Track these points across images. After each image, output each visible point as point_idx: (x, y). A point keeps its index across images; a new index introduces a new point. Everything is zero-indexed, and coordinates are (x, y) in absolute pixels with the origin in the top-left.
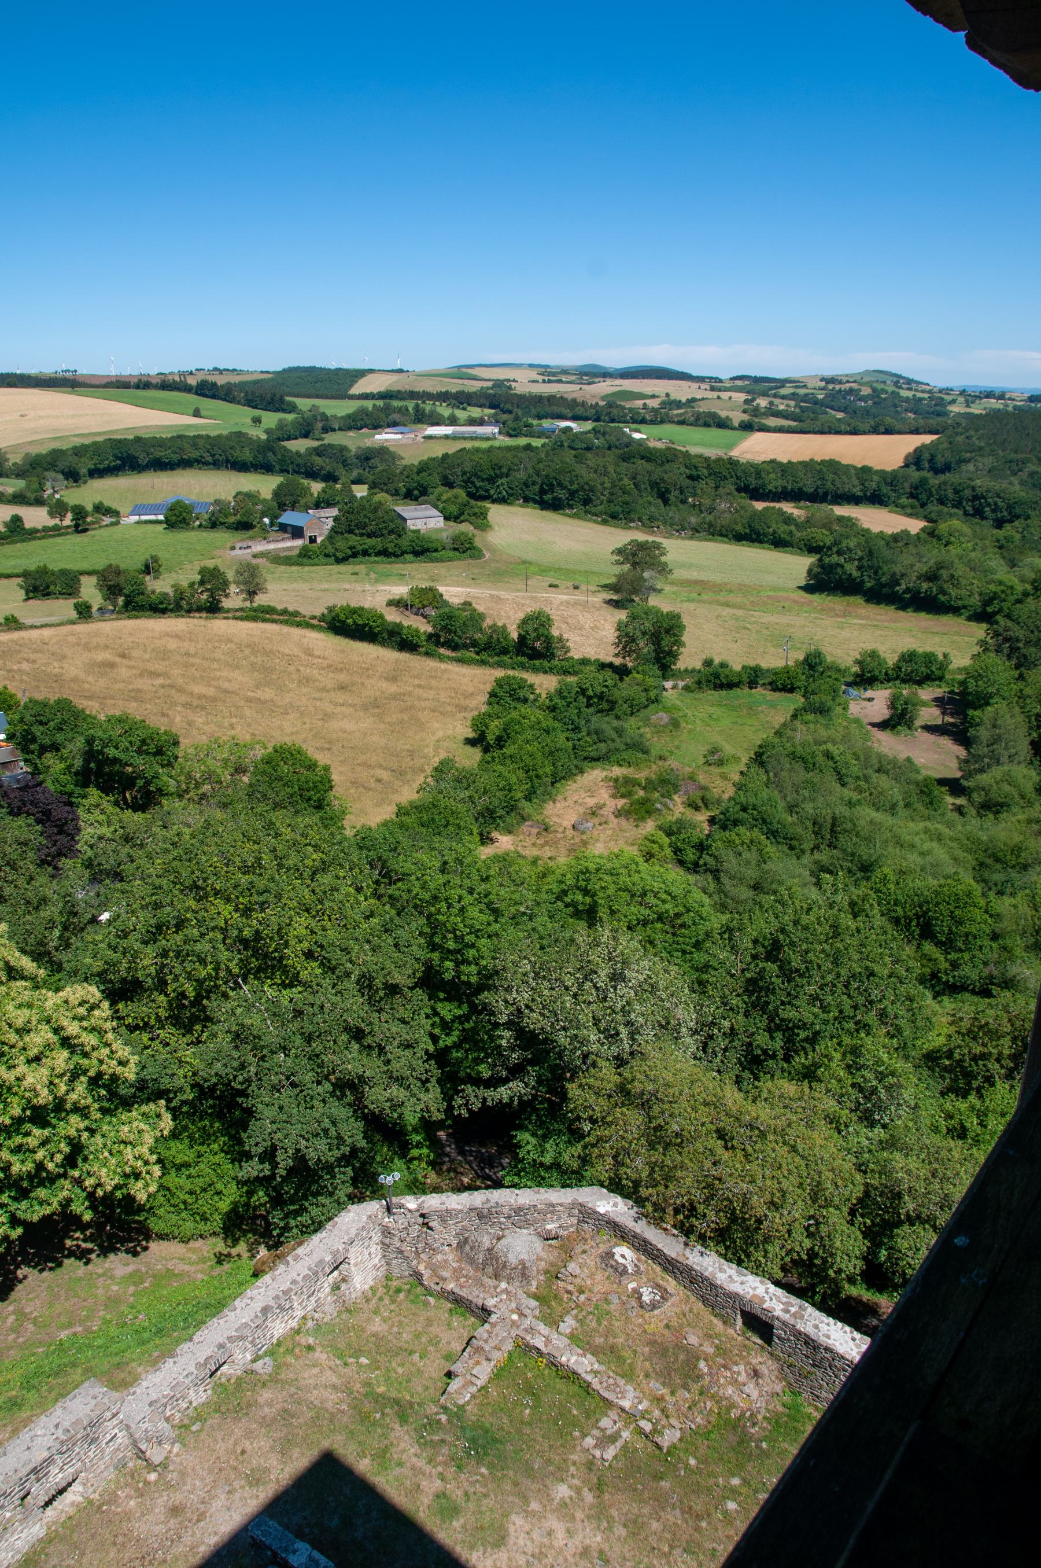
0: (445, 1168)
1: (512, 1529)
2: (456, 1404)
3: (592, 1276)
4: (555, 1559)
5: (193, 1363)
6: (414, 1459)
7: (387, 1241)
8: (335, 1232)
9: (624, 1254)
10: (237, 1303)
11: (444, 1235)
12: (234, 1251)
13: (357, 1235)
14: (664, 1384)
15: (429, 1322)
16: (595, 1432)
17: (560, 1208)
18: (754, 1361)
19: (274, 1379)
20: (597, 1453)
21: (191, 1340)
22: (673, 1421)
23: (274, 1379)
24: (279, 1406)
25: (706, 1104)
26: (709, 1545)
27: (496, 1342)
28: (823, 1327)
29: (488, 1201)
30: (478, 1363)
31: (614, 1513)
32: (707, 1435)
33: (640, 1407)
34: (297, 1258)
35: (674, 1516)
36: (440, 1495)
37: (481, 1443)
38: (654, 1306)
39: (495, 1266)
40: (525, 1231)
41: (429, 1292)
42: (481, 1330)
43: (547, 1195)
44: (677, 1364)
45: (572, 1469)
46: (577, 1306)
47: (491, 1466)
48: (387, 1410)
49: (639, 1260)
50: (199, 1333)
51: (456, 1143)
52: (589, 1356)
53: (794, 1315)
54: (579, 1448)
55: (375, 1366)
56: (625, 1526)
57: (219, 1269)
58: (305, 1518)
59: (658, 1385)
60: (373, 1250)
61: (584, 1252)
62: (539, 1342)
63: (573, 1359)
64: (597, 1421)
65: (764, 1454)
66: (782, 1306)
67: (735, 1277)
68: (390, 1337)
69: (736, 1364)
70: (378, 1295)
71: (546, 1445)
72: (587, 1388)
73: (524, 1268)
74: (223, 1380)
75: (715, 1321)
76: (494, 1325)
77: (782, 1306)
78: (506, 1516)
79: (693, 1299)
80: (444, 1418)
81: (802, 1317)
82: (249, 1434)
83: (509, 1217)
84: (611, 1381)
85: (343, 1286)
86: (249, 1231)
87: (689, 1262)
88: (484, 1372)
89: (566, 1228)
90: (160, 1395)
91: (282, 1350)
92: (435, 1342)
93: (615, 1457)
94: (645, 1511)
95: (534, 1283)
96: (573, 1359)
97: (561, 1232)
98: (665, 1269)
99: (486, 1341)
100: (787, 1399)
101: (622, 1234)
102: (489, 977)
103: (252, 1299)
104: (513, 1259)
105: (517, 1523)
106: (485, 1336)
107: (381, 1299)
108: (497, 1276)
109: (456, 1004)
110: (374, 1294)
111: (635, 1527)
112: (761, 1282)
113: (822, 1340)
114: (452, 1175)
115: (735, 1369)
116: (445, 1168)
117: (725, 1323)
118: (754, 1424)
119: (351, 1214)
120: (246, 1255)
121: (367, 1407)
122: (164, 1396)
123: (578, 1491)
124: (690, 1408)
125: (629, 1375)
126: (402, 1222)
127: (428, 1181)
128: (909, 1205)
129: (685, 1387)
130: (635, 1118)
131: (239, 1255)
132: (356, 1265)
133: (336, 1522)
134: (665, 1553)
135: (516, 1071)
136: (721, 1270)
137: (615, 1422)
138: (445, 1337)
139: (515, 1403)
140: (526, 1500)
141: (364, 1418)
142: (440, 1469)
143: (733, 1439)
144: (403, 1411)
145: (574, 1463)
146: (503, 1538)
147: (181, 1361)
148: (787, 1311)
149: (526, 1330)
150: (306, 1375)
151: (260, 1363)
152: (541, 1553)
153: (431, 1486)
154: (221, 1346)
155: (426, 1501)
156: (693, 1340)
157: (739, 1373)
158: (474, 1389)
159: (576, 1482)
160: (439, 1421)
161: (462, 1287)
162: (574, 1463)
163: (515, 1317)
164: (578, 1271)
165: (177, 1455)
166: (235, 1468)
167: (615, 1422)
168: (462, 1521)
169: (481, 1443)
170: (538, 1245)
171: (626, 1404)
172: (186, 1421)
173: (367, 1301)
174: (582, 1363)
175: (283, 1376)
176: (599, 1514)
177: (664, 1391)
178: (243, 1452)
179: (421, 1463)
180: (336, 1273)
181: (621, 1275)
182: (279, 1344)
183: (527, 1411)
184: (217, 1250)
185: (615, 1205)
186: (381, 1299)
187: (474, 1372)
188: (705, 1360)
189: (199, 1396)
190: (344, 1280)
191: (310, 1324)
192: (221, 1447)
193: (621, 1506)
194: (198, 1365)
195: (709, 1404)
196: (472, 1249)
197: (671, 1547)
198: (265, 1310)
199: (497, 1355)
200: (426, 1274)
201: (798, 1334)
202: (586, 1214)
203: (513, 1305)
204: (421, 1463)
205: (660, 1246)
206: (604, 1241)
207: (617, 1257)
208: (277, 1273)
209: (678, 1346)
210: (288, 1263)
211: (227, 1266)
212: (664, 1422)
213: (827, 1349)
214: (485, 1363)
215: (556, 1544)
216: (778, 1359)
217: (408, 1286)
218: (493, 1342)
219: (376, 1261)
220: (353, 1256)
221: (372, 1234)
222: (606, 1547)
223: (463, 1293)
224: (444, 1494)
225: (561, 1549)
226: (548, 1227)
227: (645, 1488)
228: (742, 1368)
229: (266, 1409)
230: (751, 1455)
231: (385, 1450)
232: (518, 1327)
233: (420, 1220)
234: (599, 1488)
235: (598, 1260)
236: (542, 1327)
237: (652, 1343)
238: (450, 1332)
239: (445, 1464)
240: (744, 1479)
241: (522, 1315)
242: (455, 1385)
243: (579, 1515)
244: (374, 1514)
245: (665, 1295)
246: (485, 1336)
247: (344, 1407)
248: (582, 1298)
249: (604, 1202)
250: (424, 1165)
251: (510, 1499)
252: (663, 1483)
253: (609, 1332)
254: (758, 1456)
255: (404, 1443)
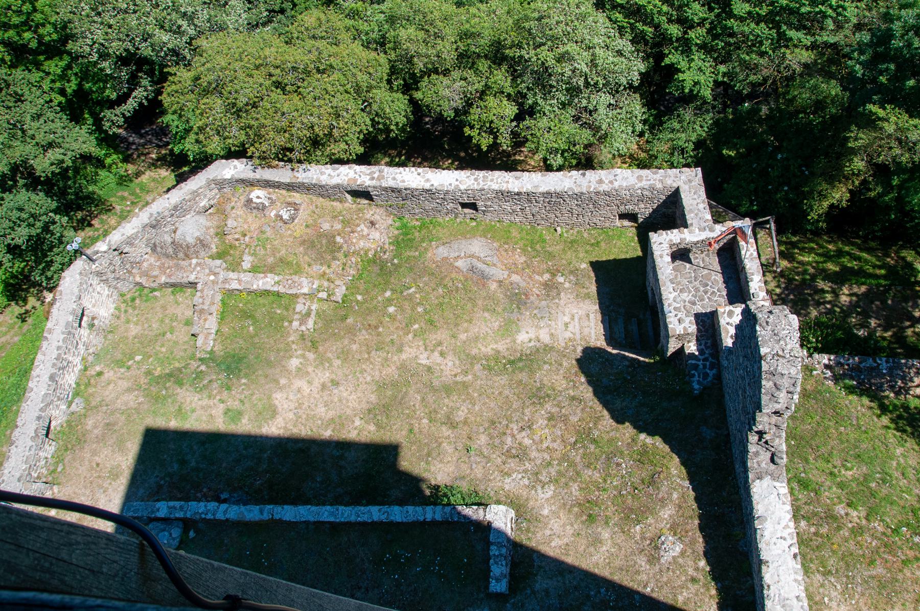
0: (135, 156)
1: (277, 402)
2: (207, 352)
3: (246, 221)
4: (309, 402)
5: (28, 440)
6: (200, 403)
7: (104, 278)
8: (64, 297)
9: (258, 195)
10: (31, 384)
11: (140, 251)
12: (29, 307)
13: (80, 291)
14: (321, 264)
15: (164, 308)
16: (296, 316)
17: (201, 190)
18: (368, 216)
19: (90, 408)
20: (303, 328)
21: (17, 427)
22: (337, 283)
23: (90, 408)
24: (102, 425)
25: (257, 67)
26: (388, 340)
27: (209, 298)
28: (399, 177)
29: (151, 215)
30: (206, 320)
31: (329, 355)
32: (360, 277)
33: (314, 287)
34: (50, 331)
35: (363, 336)
36: (227, 411)
37: (232, 365)
38: (293, 219)
39: (181, 251)
40: (188, 216)
41: (153, 290)
42: (196, 298)
43: (188, 187)
44: (324, 247)
45: (294, 346)
46: (247, 246)
47: (246, 376)
48: (168, 385)
49: (269, 193)
50: (19, 419)
51: (136, 134)
52: (269, 275)
53: (379, 179)
54: (291, 332)
55: (147, 356)
56: (338, 358)
57: (26, 327)
58: (157, 476)
59: (318, 267)
60: (99, 289)
61: (233, 208)
62: (235, 285)
63: (261, 283)
64: (294, 309)
65: (397, 267)
66: (368, 177)
67: (332, 174)
68: (146, 332)
69: (358, 225)
70: (123, 310)
71: (272, 342)
72: (278, 294)
73: (201, 241)
74: (58, 429)
75: (335, 204)
76: (202, 291)
77: (368, 177)
78: (269, 398)
79: (314, 198)
80: (203, 368)
81: (383, 177)
82: (94, 453)
83: (172, 215)
84: (290, 282)
85: (96, 322)
86: (29, 288)
87: (300, 180)
88: (212, 323)
89: (214, 198)
90: (21, 471)
91: (83, 387)
92: (174, 318)
93: (315, 323)
94: (346, 342)
95: (213, 246)
96: (261, 283)
97: (212, 202)
98: (288, 190)
99: (203, 303)
100: (398, 224)
101: (251, 184)
102: (65, 27)
103: (38, 376)
104: (191, 240)
105: (278, 398)
106: (201, 300)
107: (126, 311)
108: (187, 256)
109: (57, 58)
110: (120, 311)
111: (345, 355)
112: (350, 168)
113: (401, 185)
114: (143, 158)
115: (359, 229)
116: (135, 156)
117: (341, 202)
118: (385, 253)
119: (67, 279)
120: (38, 304)
121: (154, 389)
122: (24, 470)
123: (303, 356)
124: (343, 269)
125: (298, 271)
126: (105, 262)
127: (130, 172)
128: (419, 65)
129: (334, 258)
130: (217, 103)
131: (34, 307)
132: (94, 306)
133: (176, 466)
134: (367, 359)
135: (134, 82)
136: (322, 173)
137: (304, 304)
138: (178, 311)
139: (242, 328)
140: (277, 381)
141: (157, 399)
142: (218, 398)
143: (376, 269)
144: (176, 377)
145: (293, 342)
146: (274, 411)
147: (20, 443)
148: (373, 179)
149: (223, 282)
150: (107, 393)
151: (74, 405)
152: (300, 404)
153: (218, 411)
154: (39, 418)
155: (221, 420)
156: (326, 226)
157: (362, 230)
158: (213, 336)
159: (299, 352)
160: (201, 372)
161: (170, 276)
162: (293, 342)
163: (212, 277)
164: (235, 224)
165: (59, 492)
166: (99, 477)
167: (304, 304)
168: (247, 417)
169: (232, 365)
170: (202, 220)
171: (305, 290)
172: (52, 468)
173: (118, 318)
174: (266, 282)
175: (93, 404)
176: (322, 361)
177: (324, 268)
178: (98, 465)
179: (205, 402)
180: (85, 318)
181: (263, 210)
182: (78, 384)
183: (251, 328)
184: (16, 314)
185: (235, 167)
186: (126, 311)
187: (207, 326)
188: (339, 235)
189: (50, 449)
190: (93, 319)
191: (90, 358)
192: (83, 470)
193: (331, 348)
194: (33, 439)
195: (353, 260)
196: (162, 248)
197: (369, 353)
198: (52, 378)
199: (214, 309)
200: (143, 280)
201: (385, 189)
202: (220, 184)
203: (207, 271)
204: (205, 402)
205: (277, 180)
206: (241, 194)
207: (255, 200)
208: (43, 349)
209: (320, 235)
210: (46, 338)
211: (30, 320)
212: (332, 286)
213: (406, 189)
214: (210, 317)
215: (306, 394)
216: (382, 206)
217: (138, 296)
218: (207, 302)
219: (107, 292)
220: (87, 303)
221: (91, 281)
222: (334, 376)
223: (172, 280)
224: (228, 410)
225: (309, 394)
226: (202, 205)
227: (340, 330)
228: (362, 226)
229: (96, 431)
230: (390, 272)
231: (180, 410)
232: (217, 283)
233: (116, 253)
234: (314, 345)
235: (244, 208)
236: (232, 275)
237: (303, 242)
238: (181, 307)
239: (220, 393)
240: (392, 290)
241: (215, 274)
242: (200, 341)
243: (310, 369)
244: (195, 447)
245: (295, 207)
246: (201, 300)
247: (141, 399)
248: (247, 239)
249: (227, 169)
250: (120, 165)
251: (267, 387)
252: (348, 321)
253: (274, 250)
254: (395, 270)
255: (189, 398)
